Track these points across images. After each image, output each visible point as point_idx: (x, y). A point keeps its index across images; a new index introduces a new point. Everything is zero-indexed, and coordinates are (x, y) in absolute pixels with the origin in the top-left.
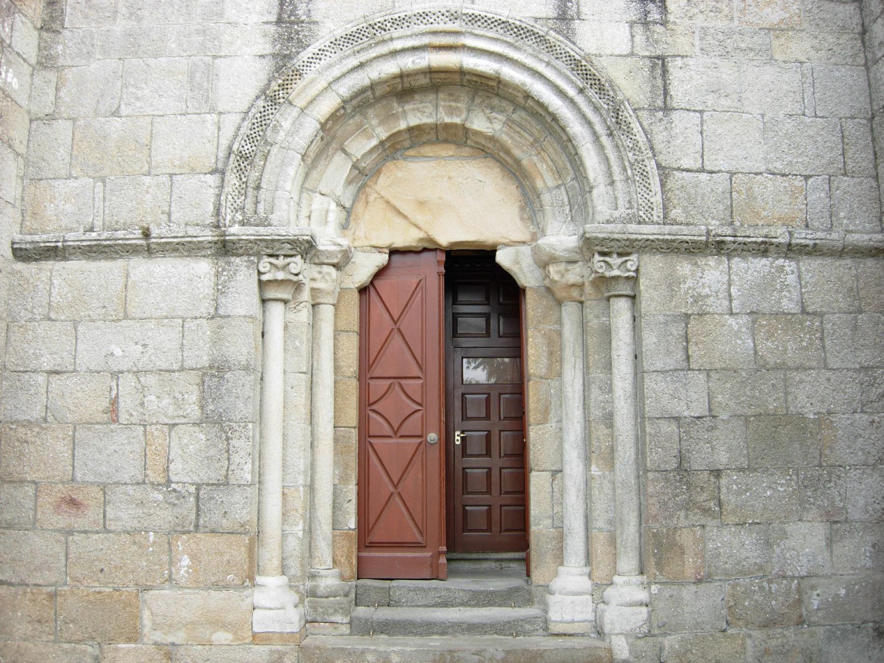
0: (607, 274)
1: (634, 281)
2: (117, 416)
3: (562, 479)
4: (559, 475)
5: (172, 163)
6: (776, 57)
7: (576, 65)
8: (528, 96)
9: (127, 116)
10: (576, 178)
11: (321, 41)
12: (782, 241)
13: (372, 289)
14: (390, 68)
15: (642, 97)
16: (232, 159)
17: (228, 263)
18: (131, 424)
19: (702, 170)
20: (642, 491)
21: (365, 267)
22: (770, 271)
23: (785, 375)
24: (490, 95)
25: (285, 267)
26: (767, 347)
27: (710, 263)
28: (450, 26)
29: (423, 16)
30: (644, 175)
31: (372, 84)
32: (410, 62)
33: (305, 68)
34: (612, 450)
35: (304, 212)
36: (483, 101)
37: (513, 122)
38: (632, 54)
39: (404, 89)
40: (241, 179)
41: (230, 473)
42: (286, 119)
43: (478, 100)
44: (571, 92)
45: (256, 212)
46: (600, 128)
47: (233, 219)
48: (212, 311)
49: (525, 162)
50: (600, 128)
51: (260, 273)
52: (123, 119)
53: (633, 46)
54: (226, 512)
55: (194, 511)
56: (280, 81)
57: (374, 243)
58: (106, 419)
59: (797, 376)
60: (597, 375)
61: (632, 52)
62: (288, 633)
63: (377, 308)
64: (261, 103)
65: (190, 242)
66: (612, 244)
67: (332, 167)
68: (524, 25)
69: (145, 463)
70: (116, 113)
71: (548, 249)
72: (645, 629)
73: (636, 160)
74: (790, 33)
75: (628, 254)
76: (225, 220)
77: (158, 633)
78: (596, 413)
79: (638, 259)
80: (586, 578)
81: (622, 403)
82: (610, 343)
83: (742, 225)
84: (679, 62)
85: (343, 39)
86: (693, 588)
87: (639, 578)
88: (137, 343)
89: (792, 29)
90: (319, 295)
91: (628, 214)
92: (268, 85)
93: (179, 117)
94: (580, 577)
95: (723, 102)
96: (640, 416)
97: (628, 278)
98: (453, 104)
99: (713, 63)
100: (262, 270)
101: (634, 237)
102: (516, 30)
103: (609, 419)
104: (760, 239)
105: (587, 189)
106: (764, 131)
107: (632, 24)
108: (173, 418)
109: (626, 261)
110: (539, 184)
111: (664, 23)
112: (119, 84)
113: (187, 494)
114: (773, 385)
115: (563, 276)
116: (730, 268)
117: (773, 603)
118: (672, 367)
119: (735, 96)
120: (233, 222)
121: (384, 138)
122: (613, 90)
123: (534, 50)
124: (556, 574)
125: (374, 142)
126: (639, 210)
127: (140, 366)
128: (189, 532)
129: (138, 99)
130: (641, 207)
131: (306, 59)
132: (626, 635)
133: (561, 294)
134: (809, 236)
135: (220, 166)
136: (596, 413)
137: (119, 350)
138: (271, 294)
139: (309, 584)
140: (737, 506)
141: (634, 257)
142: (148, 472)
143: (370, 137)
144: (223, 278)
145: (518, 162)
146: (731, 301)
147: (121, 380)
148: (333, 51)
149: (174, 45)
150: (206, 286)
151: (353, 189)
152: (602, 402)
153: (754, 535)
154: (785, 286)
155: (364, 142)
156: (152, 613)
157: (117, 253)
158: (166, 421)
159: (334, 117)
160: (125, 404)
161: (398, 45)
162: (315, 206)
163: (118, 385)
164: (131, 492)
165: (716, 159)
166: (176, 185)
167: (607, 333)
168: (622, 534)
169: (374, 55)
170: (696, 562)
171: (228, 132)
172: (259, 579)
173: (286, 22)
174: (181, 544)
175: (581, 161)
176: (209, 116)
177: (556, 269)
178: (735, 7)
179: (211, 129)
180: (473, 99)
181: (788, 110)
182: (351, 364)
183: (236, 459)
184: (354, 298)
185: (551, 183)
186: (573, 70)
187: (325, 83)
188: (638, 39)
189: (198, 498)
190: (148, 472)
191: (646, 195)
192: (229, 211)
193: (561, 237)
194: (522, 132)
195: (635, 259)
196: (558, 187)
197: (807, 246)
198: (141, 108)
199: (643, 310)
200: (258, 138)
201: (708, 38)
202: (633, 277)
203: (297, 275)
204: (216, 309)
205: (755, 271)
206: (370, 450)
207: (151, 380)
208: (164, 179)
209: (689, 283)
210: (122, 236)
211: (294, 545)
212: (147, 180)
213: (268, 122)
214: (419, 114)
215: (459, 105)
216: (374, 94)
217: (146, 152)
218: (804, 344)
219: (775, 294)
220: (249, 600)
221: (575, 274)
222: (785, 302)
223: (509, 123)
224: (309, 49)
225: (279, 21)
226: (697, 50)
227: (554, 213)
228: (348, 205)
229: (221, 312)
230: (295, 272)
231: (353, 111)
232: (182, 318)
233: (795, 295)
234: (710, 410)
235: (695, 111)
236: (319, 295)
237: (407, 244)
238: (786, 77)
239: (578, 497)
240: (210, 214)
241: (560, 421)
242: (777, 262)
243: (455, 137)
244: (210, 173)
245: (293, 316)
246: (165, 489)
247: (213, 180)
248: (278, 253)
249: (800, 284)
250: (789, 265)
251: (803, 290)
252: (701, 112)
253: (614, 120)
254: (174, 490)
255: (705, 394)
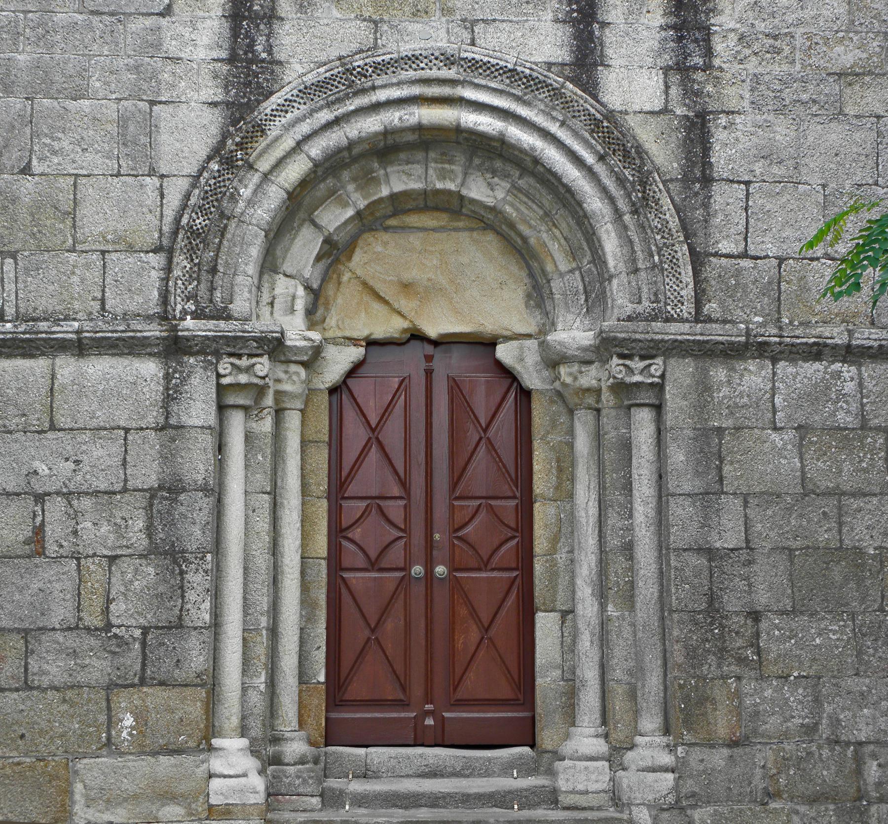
0: (628, 380)
1: (659, 388)
2: (44, 548)
3: (574, 620)
4: (570, 616)
5: (104, 237)
6: (847, 111)
7: (595, 125)
8: (536, 161)
9: (42, 175)
10: (593, 261)
11: (286, 89)
12: (840, 342)
13: (344, 388)
14: (372, 124)
15: (675, 165)
16: (180, 236)
17: (180, 363)
18: (62, 557)
19: (744, 255)
20: (667, 635)
21: (339, 361)
22: (824, 378)
23: (840, 501)
24: (492, 155)
25: (249, 369)
26: (817, 467)
27: (751, 368)
28: (445, 73)
29: (412, 60)
30: (674, 262)
31: (350, 144)
32: (394, 117)
33: (268, 123)
34: (632, 585)
35: (266, 298)
36: (483, 163)
37: (520, 190)
38: (665, 111)
39: (387, 148)
40: (192, 260)
41: (184, 613)
42: (246, 187)
43: (477, 161)
44: (589, 159)
45: (211, 301)
46: (622, 205)
47: (183, 309)
48: (162, 420)
49: (532, 241)
50: (622, 205)
51: (219, 376)
52: (36, 178)
53: (667, 101)
54: (178, 661)
55: (140, 660)
56: (238, 139)
57: (348, 334)
58: (28, 552)
59: (855, 503)
60: (616, 496)
61: (666, 107)
62: (251, 805)
63: (350, 414)
64: (214, 166)
65: (132, 338)
66: (633, 345)
67: (298, 242)
68: (535, 74)
69: (79, 604)
70: (26, 170)
71: (558, 347)
72: (671, 799)
73: (665, 244)
74: (867, 79)
75: (653, 357)
76: (174, 310)
77: (91, 811)
78: (614, 542)
79: (664, 363)
80: (602, 741)
81: (644, 532)
82: (630, 459)
83: (791, 323)
84: (723, 120)
85: (314, 87)
86: (725, 752)
87: (665, 739)
88: (67, 460)
89: (870, 73)
90: (285, 399)
91: (653, 310)
92: (222, 143)
93: (110, 178)
94: (595, 739)
95: (775, 170)
96: (663, 547)
97: (652, 384)
98: (447, 166)
99: (765, 121)
100: (222, 371)
101: (659, 337)
102: (525, 80)
103: (628, 549)
104: (812, 340)
105: (606, 276)
106: (825, 206)
107: (666, 70)
108: (113, 548)
109: (650, 365)
110: (549, 268)
111: (707, 67)
112: (28, 130)
113: (131, 640)
114: (824, 513)
115: (576, 378)
116: (774, 374)
117: (825, 773)
118: (702, 490)
119: (791, 163)
120: (184, 312)
121: (362, 207)
122: (641, 158)
123: (546, 106)
124: (567, 736)
125: (350, 212)
126: (666, 304)
127: (72, 487)
128: (133, 685)
129: (55, 153)
130: (669, 301)
131: (268, 111)
132: (649, 807)
133: (573, 400)
134: (873, 336)
135: (165, 242)
136: (614, 542)
137: (44, 467)
138: (231, 400)
139: (271, 750)
140: (779, 656)
141: (659, 361)
142: (82, 614)
143: (345, 205)
144: (174, 381)
145: (525, 240)
146: (774, 412)
147: (48, 504)
148: (302, 101)
149: (98, 84)
150: (153, 391)
151: (321, 266)
152: (622, 529)
153: (800, 691)
154: (842, 395)
155: (338, 211)
156: (85, 787)
157: (38, 349)
158: (106, 552)
159: (305, 184)
160: (55, 531)
161: (382, 95)
162: (277, 291)
163: (43, 511)
164: (61, 639)
165: (763, 242)
166: (109, 265)
167: (626, 447)
168: (644, 686)
169: (352, 108)
170: (731, 720)
171: (173, 200)
172: (216, 742)
173: (241, 61)
174: (122, 700)
175: (599, 241)
176: (148, 179)
177: (568, 370)
178: (798, 46)
179: (151, 196)
180: (471, 160)
181: (857, 179)
182: (321, 483)
183: (191, 596)
184: (323, 400)
185: (563, 267)
186: (593, 131)
187: (292, 143)
188: (674, 91)
189: (144, 644)
190: (82, 614)
191: (675, 287)
192: (179, 299)
193: (574, 333)
194: (530, 203)
195: (661, 363)
196: (571, 271)
197: (871, 347)
198: (59, 164)
199: (668, 423)
200: (213, 209)
201: (762, 87)
202: (658, 383)
203: (263, 378)
204: (167, 418)
205: (805, 377)
206: (344, 591)
207: (86, 503)
208: (94, 256)
209: (725, 391)
210: (46, 328)
211: (256, 699)
212: (73, 257)
213: (223, 189)
214: (404, 178)
215: (453, 167)
216: (350, 154)
217: (69, 222)
218: (864, 465)
219: (829, 404)
220: (205, 765)
221: (590, 377)
222: (840, 415)
223: (515, 189)
224: (273, 99)
225: (232, 59)
226: (746, 104)
227: (566, 304)
228: (315, 286)
229: (173, 421)
230: (261, 374)
231: (324, 173)
232: (124, 428)
233: (854, 407)
234: (747, 541)
235: (739, 182)
236: (285, 399)
237: (388, 335)
238: (858, 136)
239: (592, 642)
240: (155, 302)
241: (571, 551)
242: (833, 367)
243: (452, 206)
244: (152, 251)
245: (254, 425)
246: (104, 635)
247: (156, 260)
248: (241, 352)
249: (861, 393)
250: (848, 371)
251: (865, 400)
252: (747, 183)
253: (640, 195)
254: (116, 636)
255: (741, 522)
